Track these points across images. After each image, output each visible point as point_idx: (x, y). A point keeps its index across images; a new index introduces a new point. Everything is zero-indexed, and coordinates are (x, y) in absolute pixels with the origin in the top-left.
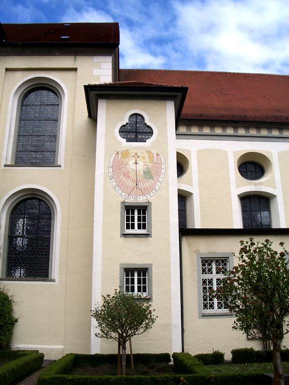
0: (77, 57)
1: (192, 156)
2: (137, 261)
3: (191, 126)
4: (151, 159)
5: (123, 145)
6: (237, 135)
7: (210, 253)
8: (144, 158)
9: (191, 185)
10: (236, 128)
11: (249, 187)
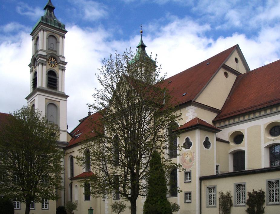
0: (181, 110)
1: (245, 132)
2: (188, 190)
3: (240, 117)
4: (191, 155)
5: (184, 151)
6: (266, 114)
7: (210, 186)
8: (189, 155)
9: (244, 147)
10: (265, 111)
11: (269, 142)
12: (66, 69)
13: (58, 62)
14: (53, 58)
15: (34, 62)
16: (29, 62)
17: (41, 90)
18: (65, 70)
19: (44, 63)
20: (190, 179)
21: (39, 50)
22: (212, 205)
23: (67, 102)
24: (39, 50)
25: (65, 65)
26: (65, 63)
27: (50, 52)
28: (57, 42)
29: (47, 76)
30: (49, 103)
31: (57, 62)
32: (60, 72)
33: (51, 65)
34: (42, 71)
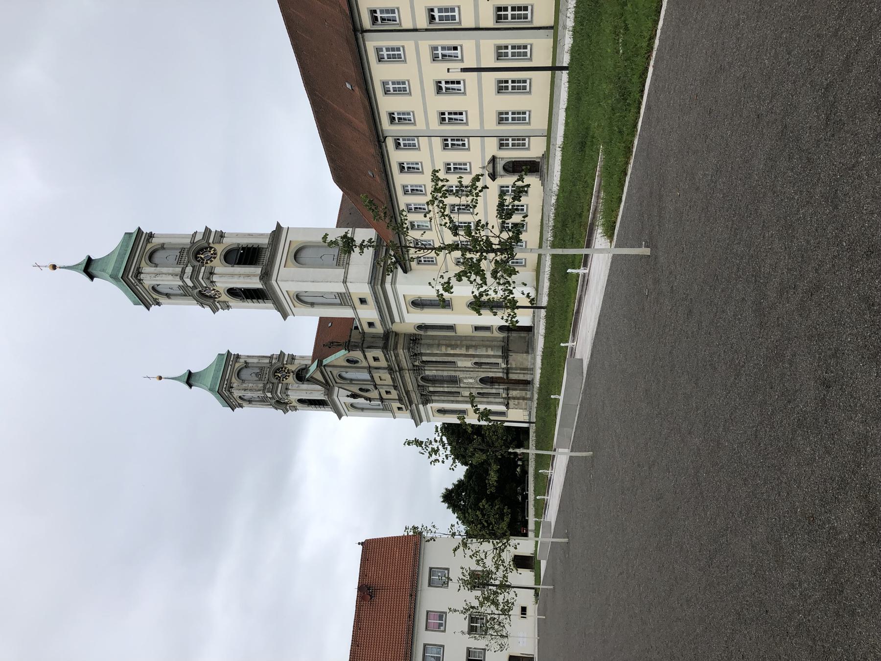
12: (219, 230)
13: (282, 366)
14: (198, 256)
15: (282, 404)
16: (208, 310)
17: (266, 276)
18: (292, 355)
19: (208, 270)
20: (466, 165)
21: (181, 283)
22: (456, 14)
23: (291, 228)
24: (181, 283)
25: (210, 231)
26: (207, 231)
27: (185, 259)
28: (162, 247)
29: (305, 383)
30: (299, 265)
31: (282, 368)
32: (296, 362)
33: (288, 377)
34: (298, 391)
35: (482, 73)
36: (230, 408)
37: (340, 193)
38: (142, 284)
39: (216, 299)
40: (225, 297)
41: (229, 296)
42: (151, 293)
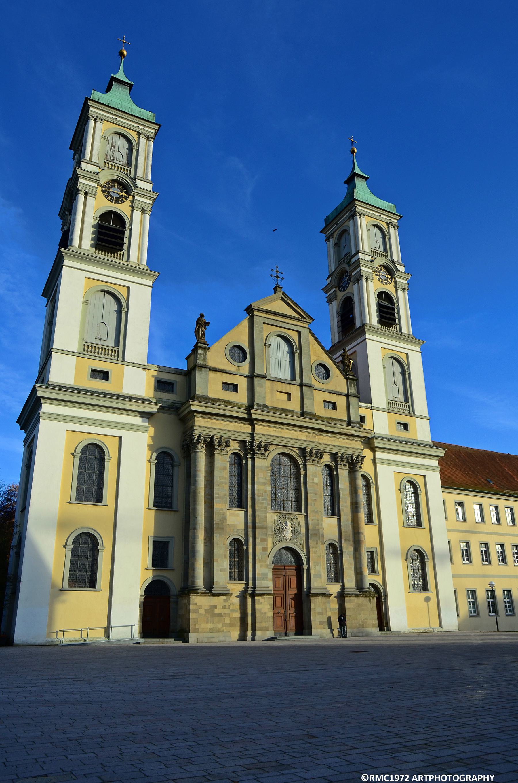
33: (380, 281)
35: (214, 581)
36: (324, 226)
37: (372, 453)
38: (349, 218)
39: (337, 288)
40: (341, 295)
41: (343, 300)
42: (338, 231)
